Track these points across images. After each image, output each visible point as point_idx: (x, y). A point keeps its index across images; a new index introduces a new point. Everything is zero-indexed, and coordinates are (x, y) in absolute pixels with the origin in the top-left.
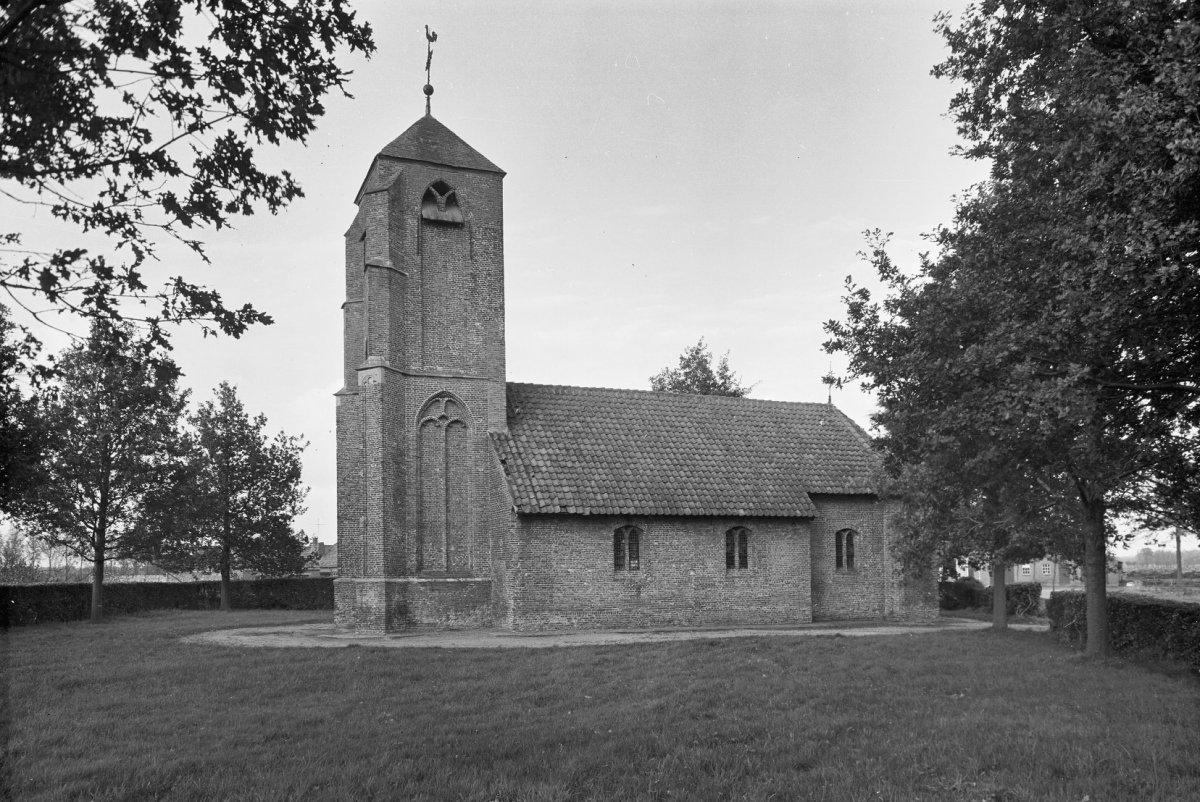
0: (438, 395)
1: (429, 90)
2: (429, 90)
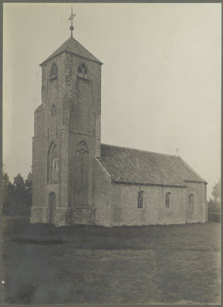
0: (81, 142)
1: (72, 28)
2: (72, 28)
